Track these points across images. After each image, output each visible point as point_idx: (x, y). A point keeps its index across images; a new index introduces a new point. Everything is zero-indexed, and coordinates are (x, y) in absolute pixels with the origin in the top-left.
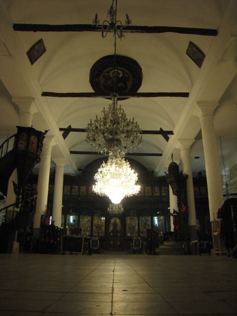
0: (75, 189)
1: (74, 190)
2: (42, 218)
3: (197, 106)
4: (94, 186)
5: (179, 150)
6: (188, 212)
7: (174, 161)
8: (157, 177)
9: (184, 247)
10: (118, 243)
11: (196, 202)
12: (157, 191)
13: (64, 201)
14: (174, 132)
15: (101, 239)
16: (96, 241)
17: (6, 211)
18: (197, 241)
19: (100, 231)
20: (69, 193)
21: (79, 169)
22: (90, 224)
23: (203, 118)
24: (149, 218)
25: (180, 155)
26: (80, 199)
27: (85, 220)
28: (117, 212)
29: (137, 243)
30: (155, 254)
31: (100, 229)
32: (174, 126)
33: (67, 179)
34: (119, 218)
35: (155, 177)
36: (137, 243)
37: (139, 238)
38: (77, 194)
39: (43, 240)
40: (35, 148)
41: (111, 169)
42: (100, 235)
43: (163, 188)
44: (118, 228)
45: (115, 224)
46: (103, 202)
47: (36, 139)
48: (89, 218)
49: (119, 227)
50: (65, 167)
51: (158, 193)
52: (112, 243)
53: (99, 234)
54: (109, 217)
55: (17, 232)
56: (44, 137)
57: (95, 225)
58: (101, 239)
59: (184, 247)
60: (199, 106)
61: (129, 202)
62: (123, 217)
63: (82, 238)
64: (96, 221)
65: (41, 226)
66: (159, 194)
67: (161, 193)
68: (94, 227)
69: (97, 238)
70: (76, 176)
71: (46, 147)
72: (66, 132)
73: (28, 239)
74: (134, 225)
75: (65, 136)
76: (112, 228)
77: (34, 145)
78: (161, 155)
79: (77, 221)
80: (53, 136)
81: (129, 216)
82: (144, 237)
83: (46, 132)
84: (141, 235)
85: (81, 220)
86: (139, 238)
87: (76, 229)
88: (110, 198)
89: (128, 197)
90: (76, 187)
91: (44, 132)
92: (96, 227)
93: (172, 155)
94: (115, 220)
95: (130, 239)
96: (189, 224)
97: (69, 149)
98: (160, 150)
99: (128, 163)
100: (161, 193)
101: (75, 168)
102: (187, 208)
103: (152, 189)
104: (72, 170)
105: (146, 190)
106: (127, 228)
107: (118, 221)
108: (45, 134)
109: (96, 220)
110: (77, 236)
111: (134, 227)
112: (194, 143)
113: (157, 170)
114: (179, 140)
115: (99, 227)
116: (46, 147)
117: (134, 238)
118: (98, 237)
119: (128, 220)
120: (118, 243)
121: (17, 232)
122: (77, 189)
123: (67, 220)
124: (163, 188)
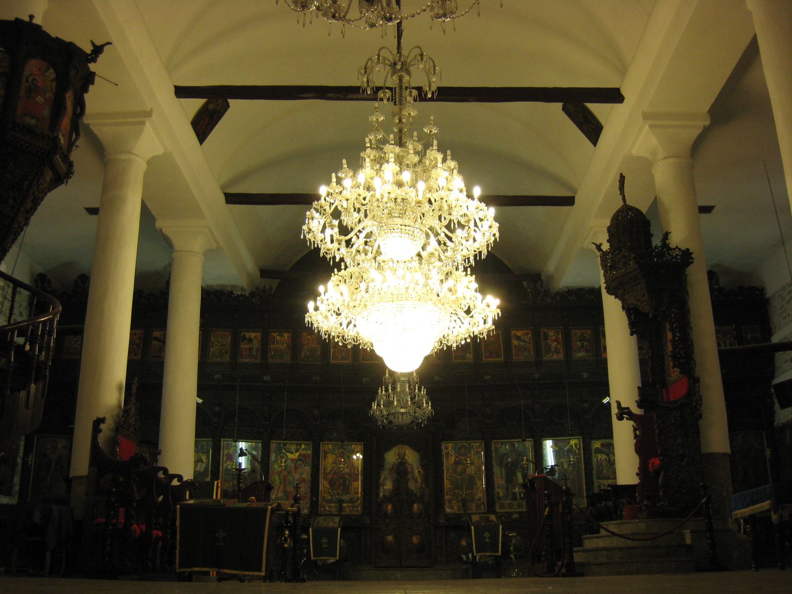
0: (250, 340)
1: (244, 346)
2: (96, 430)
3: (647, 128)
4: (311, 305)
5: (645, 165)
6: (700, 402)
7: (629, 202)
9: (688, 541)
10: (415, 539)
11: (723, 366)
12: (554, 344)
13: (206, 384)
14: (624, 92)
15: (350, 526)
16: (330, 533)
18: (765, 505)
19: (344, 497)
20: (227, 358)
21: (265, 273)
22: (306, 472)
23: (671, 160)
24: (529, 444)
25: (652, 177)
26: (267, 378)
27: (290, 456)
28: (407, 420)
29: (325, 540)
30: (573, 571)
31: (346, 488)
32: (623, 71)
33: (217, 305)
34: (416, 447)
36: (487, 535)
37: (493, 517)
38: (258, 361)
39: (101, 520)
40: (46, 113)
41: (377, 183)
42: (347, 508)
43: (576, 333)
44: (412, 485)
45: (401, 470)
46: (357, 368)
47: (51, 74)
48: (305, 449)
49: (416, 482)
50: (210, 254)
51: (557, 351)
52: (390, 538)
53: (341, 508)
54: (378, 438)
56: (89, 78)
57: (326, 474)
58: (350, 526)
59: (688, 541)
60: (651, 126)
61: (453, 372)
62: (427, 438)
63: (267, 509)
64: (328, 462)
65: (92, 465)
66: (561, 356)
67: (568, 351)
68: (323, 484)
69: (334, 522)
71: (124, 157)
72: (210, 106)
73: (37, 518)
74: (471, 470)
75: (203, 125)
76: (388, 486)
77: (40, 99)
78: (569, 201)
79: (263, 462)
80: (149, 114)
81: (450, 438)
82: (509, 514)
83: (98, 50)
84: (498, 509)
85: (273, 457)
86: (493, 517)
87: (257, 484)
88: (379, 352)
89: (449, 348)
90: (253, 335)
91: (88, 49)
92: (332, 483)
93: (622, 179)
94: (402, 457)
95: (459, 525)
96: (704, 450)
97: (223, 188)
98: (556, 180)
99: (452, 164)
100: (568, 351)
101: (251, 266)
102: (694, 382)
103: (536, 337)
104: (237, 272)
105: (515, 342)
106: (446, 483)
107: (412, 457)
108: (94, 60)
109: (331, 458)
110: (245, 505)
111: (471, 482)
112: (706, 131)
113: (551, 267)
114: (646, 116)
115: (341, 482)
116: (124, 157)
117: (475, 518)
118: (337, 519)
119: (449, 450)
120: (415, 539)
121: (311, 529)
122: (256, 344)
123: (222, 458)
124: (576, 333)
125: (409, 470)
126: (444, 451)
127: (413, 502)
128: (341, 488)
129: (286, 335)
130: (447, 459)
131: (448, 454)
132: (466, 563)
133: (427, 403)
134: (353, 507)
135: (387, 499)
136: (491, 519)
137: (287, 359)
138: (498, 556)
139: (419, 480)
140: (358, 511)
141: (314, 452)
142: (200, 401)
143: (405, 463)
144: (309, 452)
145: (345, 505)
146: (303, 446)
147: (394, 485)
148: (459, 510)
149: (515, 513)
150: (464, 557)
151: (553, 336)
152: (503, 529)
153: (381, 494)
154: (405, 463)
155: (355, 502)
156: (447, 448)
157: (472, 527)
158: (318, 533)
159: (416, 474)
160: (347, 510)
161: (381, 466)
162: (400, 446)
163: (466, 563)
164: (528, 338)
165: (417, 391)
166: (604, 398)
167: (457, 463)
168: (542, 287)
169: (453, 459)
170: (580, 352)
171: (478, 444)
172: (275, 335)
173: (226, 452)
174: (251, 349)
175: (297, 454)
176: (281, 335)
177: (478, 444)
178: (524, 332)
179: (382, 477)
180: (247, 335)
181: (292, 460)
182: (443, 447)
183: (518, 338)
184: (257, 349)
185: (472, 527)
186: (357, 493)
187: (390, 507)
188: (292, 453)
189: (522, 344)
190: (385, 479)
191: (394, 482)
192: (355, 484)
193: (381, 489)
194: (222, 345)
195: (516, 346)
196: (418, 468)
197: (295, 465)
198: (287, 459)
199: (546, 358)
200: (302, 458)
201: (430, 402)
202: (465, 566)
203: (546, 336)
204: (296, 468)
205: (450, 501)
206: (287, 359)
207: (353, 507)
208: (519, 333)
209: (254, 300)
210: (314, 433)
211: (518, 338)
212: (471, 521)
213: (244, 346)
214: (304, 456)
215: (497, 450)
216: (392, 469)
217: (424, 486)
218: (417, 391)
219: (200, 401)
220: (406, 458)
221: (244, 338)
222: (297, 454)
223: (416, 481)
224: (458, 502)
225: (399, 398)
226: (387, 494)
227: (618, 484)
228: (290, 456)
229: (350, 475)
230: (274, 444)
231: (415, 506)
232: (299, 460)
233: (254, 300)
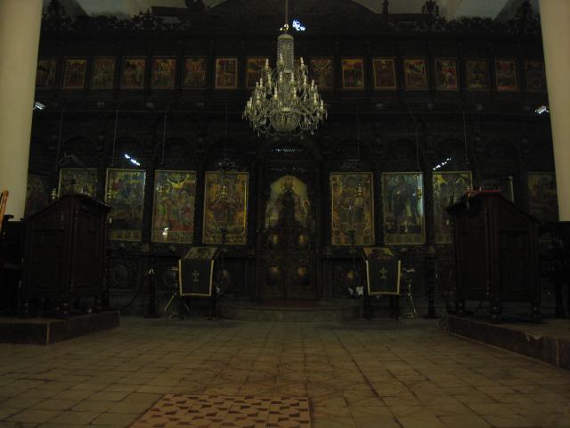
0: (134, 67)
8: (449, 19)
10: (301, 271)
12: (448, 74)
15: (228, 258)
17: (218, 250)
19: (229, 228)
20: (110, 86)
26: (150, 105)
28: (292, 124)
29: (196, 274)
35: (442, 21)
36: (383, 271)
44: (298, 216)
45: (287, 201)
48: (189, 178)
49: (302, 214)
51: (451, 81)
52: (275, 270)
55: (180, 261)
68: (209, 215)
70: (136, 19)
81: (338, 170)
85: (158, 188)
90: (136, 62)
105: (408, 71)
107: (299, 188)
109: (215, 188)
115: (227, 210)
119: (339, 185)
120: (301, 271)
121: (180, 261)
122: (140, 70)
125: (296, 201)
126: (332, 183)
127: (299, 234)
128: (226, 218)
129: (170, 61)
130: (335, 191)
131: (336, 185)
132: (353, 297)
133: (318, 100)
134: (237, 238)
135: (273, 230)
136: (386, 252)
137: (171, 85)
138: (397, 296)
139: (306, 211)
140: (512, 65)
141: (198, 181)
142: (40, 107)
143: (291, 194)
144: (194, 182)
145: (229, 235)
146: (188, 176)
147: (280, 215)
148: (346, 242)
149: (404, 246)
150: (351, 290)
151: (447, 67)
152: (402, 267)
153: (267, 225)
154: (291, 194)
155: (240, 232)
156: (334, 179)
157: (367, 262)
158: (188, 267)
159: (303, 203)
160: (231, 240)
161: (267, 197)
162: (287, 176)
163: (353, 297)
164: (421, 67)
165: (305, 83)
166: (538, 107)
167: (344, 195)
168: (437, 15)
169: (341, 190)
170: (475, 83)
171: (366, 176)
172: (159, 61)
173: (112, 181)
174: (133, 76)
175: (182, 184)
176: (165, 62)
177: (366, 176)
178: (418, 61)
179: (268, 207)
180: (131, 62)
181: (177, 189)
182: (331, 178)
183: (411, 67)
184: (141, 76)
185: (367, 262)
186: (242, 223)
187: (275, 238)
188: (176, 182)
189: (415, 72)
190: (271, 209)
191: (280, 213)
192: (240, 214)
193: (267, 220)
194: (106, 72)
195: (409, 75)
196: (305, 199)
197: (180, 194)
198: (171, 188)
199: (440, 88)
200: (187, 188)
201: (322, 102)
202: (352, 303)
203: (440, 67)
204: (180, 198)
205: (337, 233)
206: (171, 85)
207: (237, 238)
208: (412, 62)
209: (138, 25)
210: (201, 163)
211: (411, 67)
212: (365, 255)
213: (128, 73)
214: (188, 185)
215: (386, 182)
216: (278, 200)
217: (311, 217)
218: (305, 83)
219: (40, 107)
220: (293, 188)
221: (128, 64)
222: (182, 184)
223: (303, 212)
224: (346, 234)
225: (280, 91)
226: (273, 225)
227: (561, 220)
228: (175, 185)
229: (234, 205)
230: (158, 173)
231: (301, 237)
232: (182, 189)
233: (138, 25)
